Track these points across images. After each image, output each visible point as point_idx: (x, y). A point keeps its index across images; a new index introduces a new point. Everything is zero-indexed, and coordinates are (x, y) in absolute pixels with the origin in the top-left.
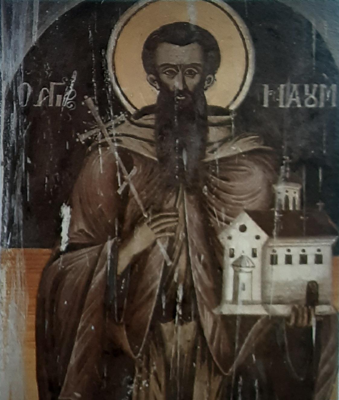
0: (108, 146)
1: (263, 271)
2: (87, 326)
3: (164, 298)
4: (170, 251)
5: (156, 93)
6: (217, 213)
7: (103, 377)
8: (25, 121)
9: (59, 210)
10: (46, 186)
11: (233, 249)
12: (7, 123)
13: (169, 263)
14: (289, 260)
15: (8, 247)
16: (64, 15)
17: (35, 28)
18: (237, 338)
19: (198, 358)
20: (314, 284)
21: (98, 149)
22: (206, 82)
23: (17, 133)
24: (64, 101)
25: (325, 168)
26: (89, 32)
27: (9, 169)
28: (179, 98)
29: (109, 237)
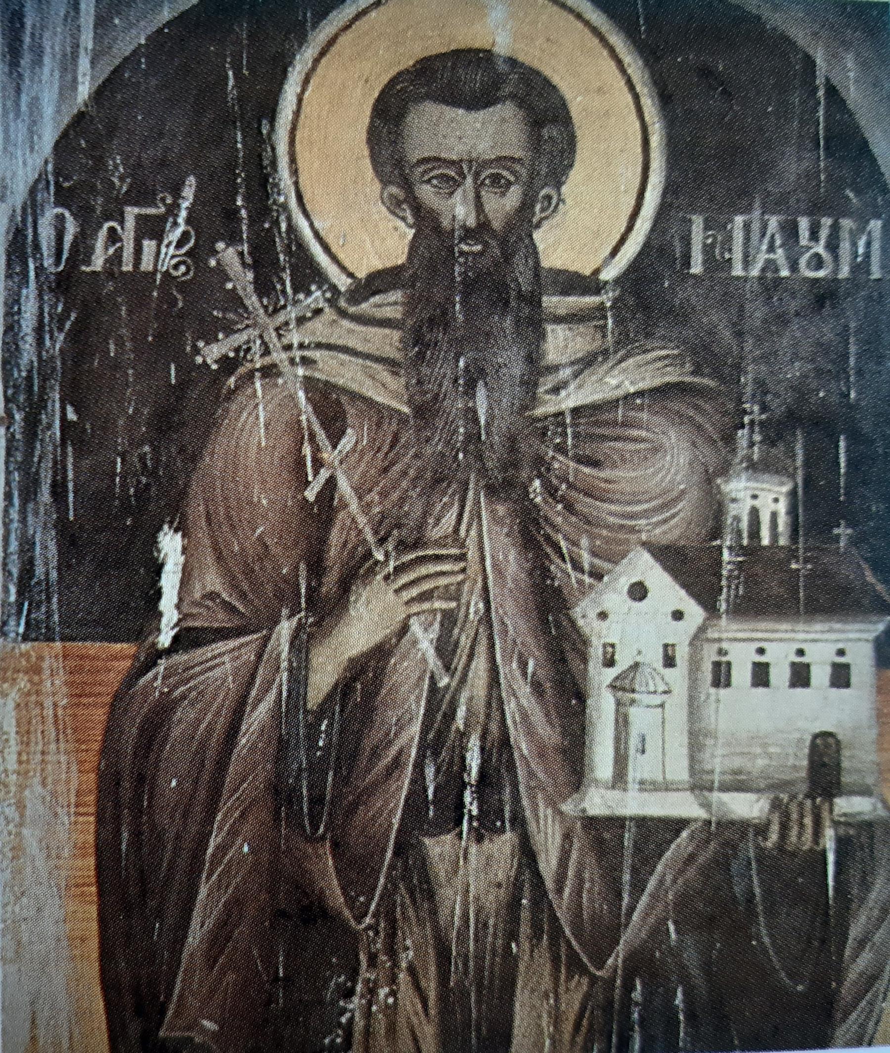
0: (279, 374)
1: (696, 713)
2: (232, 842)
3: (430, 772)
4: (446, 649)
5: (403, 236)
6: (570, 552)
7: (276, 979)
8: (60, 309)
9: (153, 542)
10: (118, 479)
11: (613, 646)
12: (13, 315)
13: (444, 681)
14: (761, 675)
15: (20, 638)
16: (160, 31)
17: (84, 63)
18: (626, 877)
19: (525, 929)
20: (831, 740)
21: (253, 383)
22: (538, 207)
23: (40, 342)
24: (162, 256)
25: (855, 437)
26: (227, 74)
27: (18, 436)
28: (465, 248)
29: (285, 612)
